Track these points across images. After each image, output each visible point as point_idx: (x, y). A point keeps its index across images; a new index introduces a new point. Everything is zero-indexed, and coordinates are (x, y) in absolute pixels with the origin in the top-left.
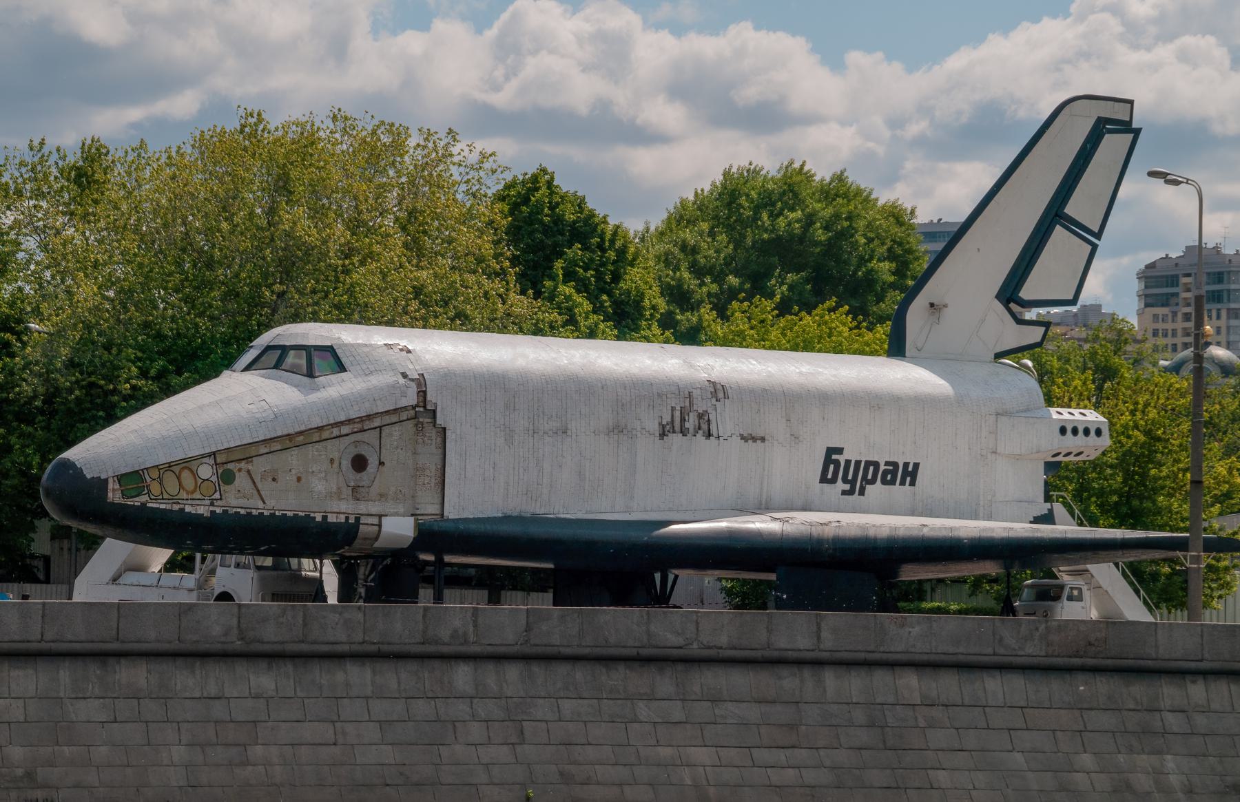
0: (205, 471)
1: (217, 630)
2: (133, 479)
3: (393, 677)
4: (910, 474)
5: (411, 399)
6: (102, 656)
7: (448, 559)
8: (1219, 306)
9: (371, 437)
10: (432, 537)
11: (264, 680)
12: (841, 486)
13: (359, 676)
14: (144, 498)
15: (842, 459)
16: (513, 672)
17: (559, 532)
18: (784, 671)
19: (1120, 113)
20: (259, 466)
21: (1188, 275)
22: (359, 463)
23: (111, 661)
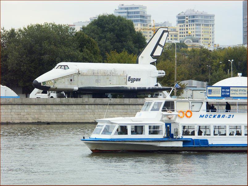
0: (53, 81)
1: (58, 102)
2: (44, 83)
3: (79, 107)
4: (139, 80)
5: (78, 72)
6: (45, 105)
7: (81, 92)
8: (194, 23)
9: (73, 77)
10: (80, 89)
11: (64, 107)
12: (131, 81)
13: (75, 107)
14: (45, 85)
15: (131, 78)
16: (93, 106)
17: (110, 89)
18: (125, 106)
19: (166, 29)
20: (59, 81)
21: (187, 16)
22: (71, 80)
23: (46, 105)
